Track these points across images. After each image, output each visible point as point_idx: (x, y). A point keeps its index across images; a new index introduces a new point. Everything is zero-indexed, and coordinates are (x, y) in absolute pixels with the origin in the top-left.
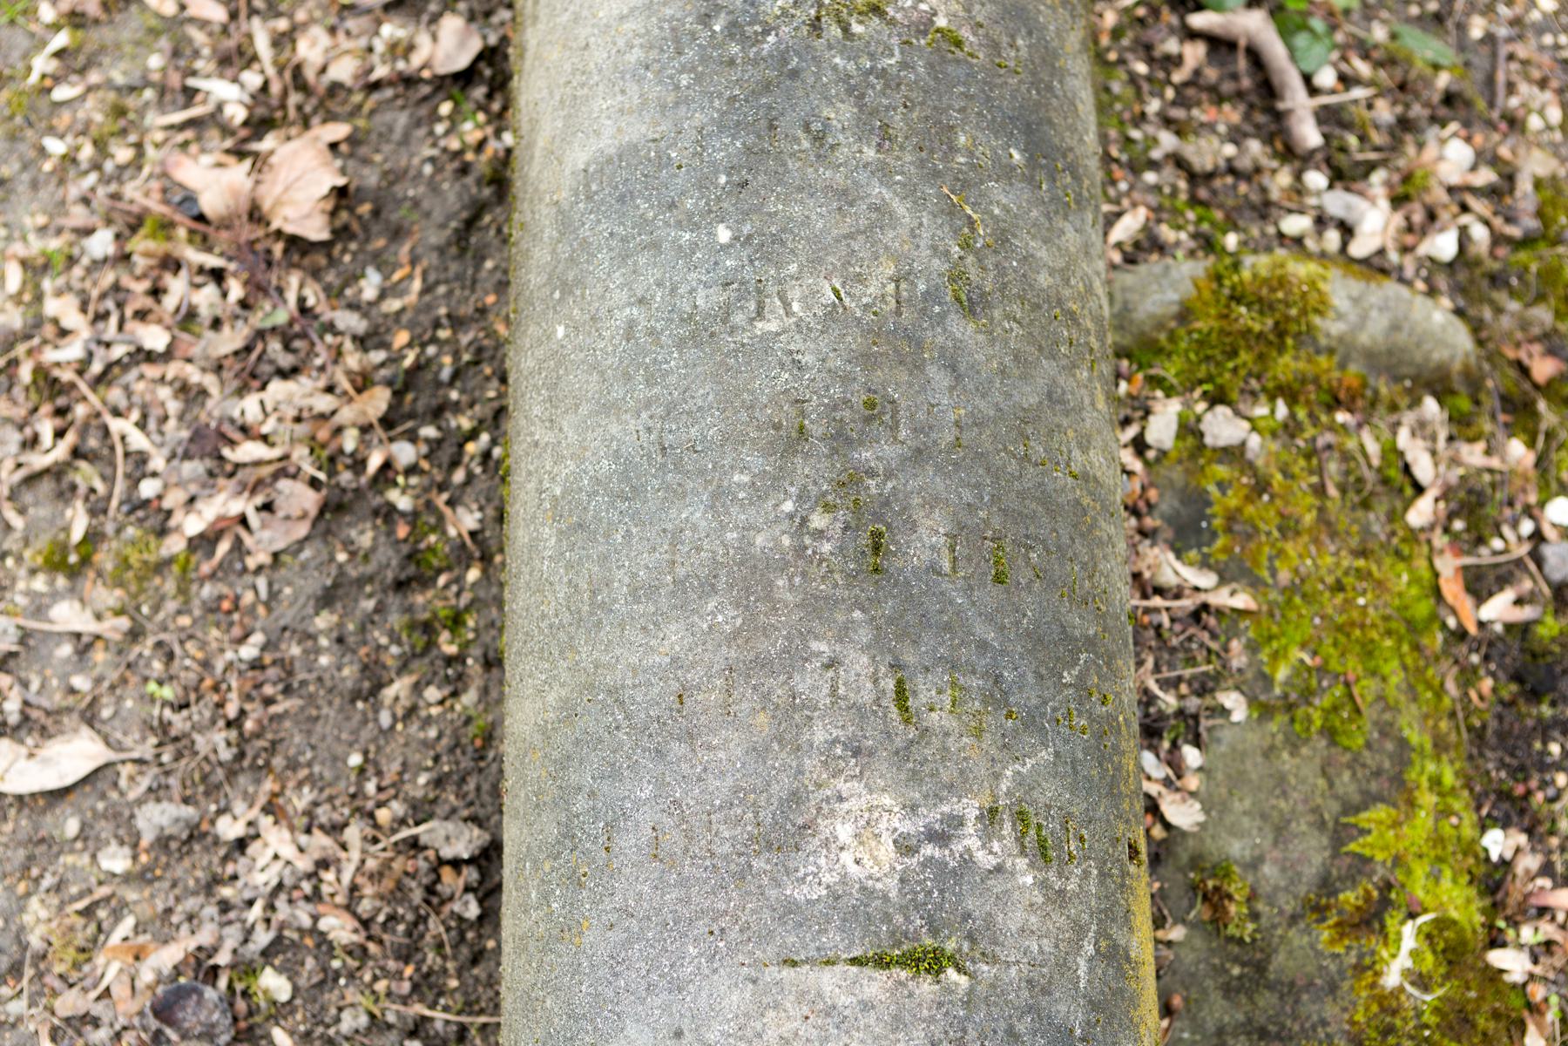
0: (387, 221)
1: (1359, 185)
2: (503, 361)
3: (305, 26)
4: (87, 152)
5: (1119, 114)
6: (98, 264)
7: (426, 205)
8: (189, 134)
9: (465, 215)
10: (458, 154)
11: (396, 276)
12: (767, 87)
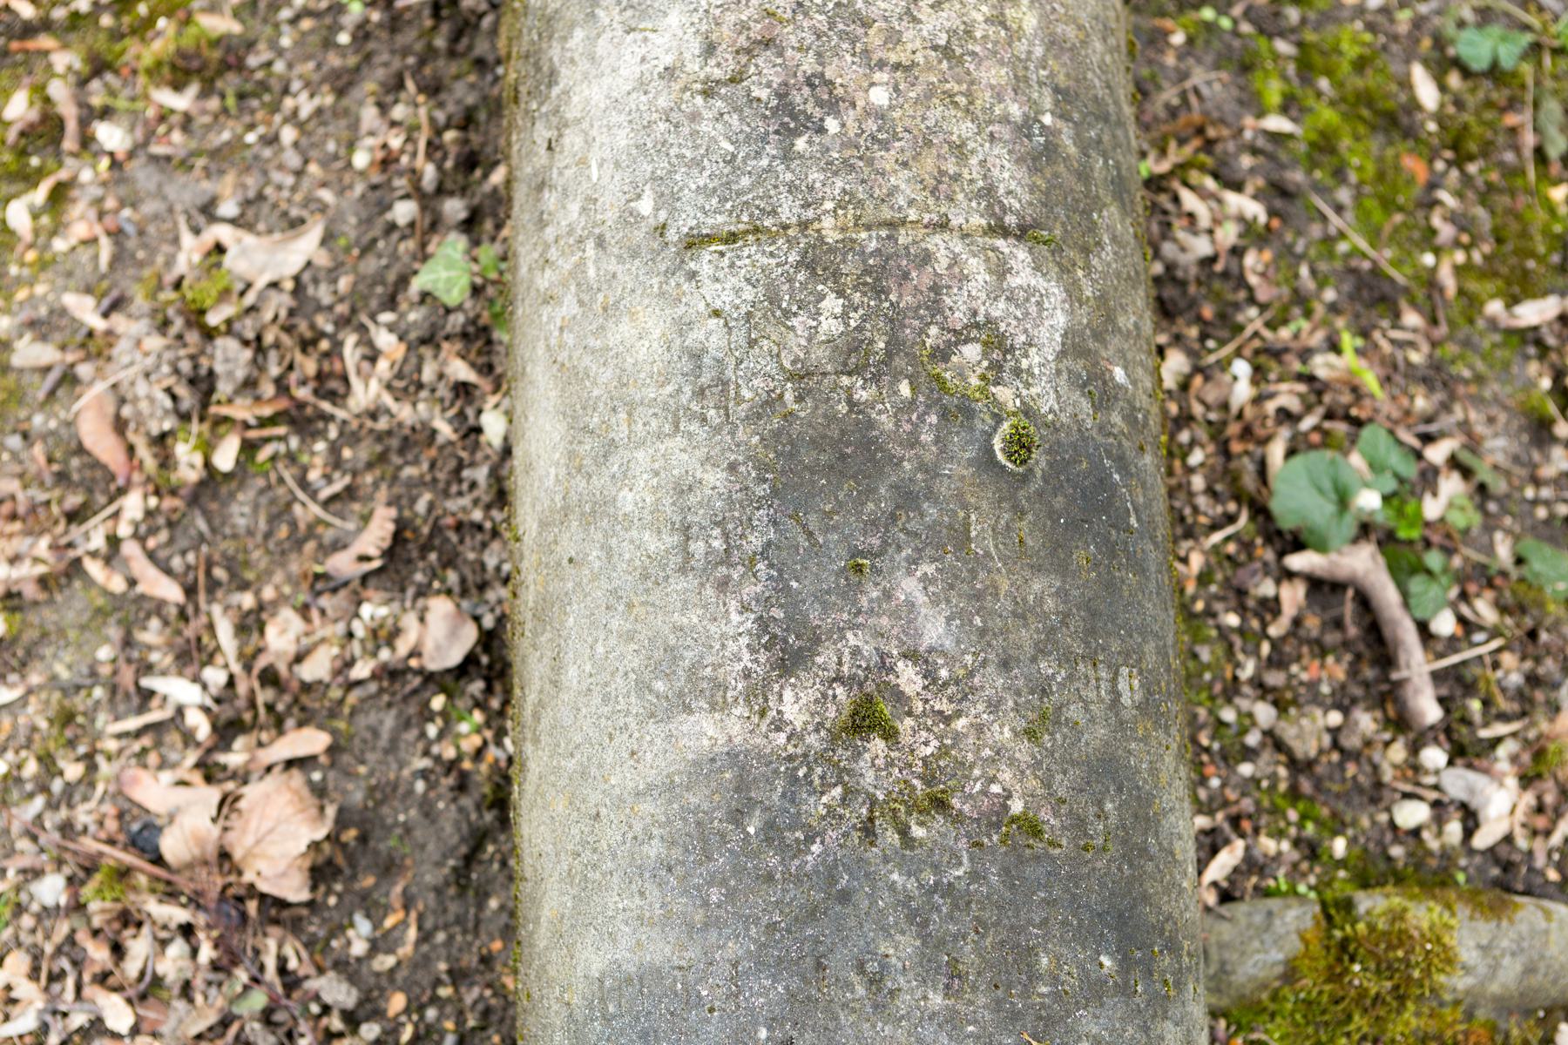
0: (376, 853)
1: (1484, 763)
2: (513, 1027)
3: (275, 604)
4: (31, 768)
5: (1210, 686)
6: (47, 912)
7: (418, 834)
8: (146, 741)
9: (464, 850)
10: (451, 766)
11: (389, 922)
12: (812, 914)
